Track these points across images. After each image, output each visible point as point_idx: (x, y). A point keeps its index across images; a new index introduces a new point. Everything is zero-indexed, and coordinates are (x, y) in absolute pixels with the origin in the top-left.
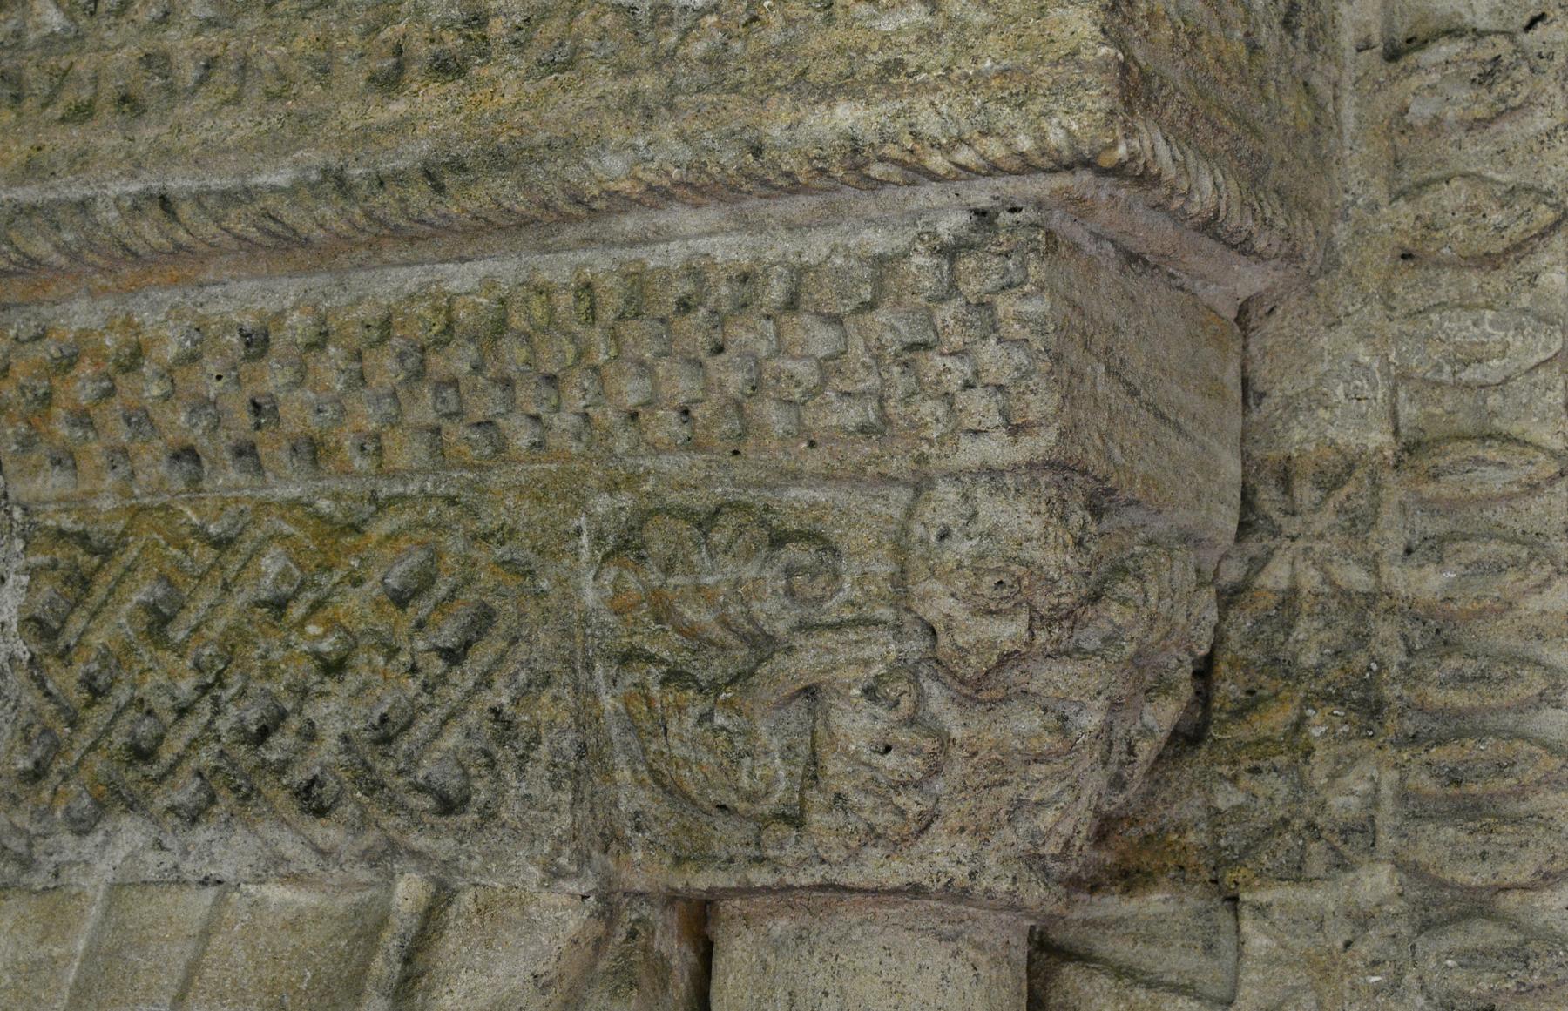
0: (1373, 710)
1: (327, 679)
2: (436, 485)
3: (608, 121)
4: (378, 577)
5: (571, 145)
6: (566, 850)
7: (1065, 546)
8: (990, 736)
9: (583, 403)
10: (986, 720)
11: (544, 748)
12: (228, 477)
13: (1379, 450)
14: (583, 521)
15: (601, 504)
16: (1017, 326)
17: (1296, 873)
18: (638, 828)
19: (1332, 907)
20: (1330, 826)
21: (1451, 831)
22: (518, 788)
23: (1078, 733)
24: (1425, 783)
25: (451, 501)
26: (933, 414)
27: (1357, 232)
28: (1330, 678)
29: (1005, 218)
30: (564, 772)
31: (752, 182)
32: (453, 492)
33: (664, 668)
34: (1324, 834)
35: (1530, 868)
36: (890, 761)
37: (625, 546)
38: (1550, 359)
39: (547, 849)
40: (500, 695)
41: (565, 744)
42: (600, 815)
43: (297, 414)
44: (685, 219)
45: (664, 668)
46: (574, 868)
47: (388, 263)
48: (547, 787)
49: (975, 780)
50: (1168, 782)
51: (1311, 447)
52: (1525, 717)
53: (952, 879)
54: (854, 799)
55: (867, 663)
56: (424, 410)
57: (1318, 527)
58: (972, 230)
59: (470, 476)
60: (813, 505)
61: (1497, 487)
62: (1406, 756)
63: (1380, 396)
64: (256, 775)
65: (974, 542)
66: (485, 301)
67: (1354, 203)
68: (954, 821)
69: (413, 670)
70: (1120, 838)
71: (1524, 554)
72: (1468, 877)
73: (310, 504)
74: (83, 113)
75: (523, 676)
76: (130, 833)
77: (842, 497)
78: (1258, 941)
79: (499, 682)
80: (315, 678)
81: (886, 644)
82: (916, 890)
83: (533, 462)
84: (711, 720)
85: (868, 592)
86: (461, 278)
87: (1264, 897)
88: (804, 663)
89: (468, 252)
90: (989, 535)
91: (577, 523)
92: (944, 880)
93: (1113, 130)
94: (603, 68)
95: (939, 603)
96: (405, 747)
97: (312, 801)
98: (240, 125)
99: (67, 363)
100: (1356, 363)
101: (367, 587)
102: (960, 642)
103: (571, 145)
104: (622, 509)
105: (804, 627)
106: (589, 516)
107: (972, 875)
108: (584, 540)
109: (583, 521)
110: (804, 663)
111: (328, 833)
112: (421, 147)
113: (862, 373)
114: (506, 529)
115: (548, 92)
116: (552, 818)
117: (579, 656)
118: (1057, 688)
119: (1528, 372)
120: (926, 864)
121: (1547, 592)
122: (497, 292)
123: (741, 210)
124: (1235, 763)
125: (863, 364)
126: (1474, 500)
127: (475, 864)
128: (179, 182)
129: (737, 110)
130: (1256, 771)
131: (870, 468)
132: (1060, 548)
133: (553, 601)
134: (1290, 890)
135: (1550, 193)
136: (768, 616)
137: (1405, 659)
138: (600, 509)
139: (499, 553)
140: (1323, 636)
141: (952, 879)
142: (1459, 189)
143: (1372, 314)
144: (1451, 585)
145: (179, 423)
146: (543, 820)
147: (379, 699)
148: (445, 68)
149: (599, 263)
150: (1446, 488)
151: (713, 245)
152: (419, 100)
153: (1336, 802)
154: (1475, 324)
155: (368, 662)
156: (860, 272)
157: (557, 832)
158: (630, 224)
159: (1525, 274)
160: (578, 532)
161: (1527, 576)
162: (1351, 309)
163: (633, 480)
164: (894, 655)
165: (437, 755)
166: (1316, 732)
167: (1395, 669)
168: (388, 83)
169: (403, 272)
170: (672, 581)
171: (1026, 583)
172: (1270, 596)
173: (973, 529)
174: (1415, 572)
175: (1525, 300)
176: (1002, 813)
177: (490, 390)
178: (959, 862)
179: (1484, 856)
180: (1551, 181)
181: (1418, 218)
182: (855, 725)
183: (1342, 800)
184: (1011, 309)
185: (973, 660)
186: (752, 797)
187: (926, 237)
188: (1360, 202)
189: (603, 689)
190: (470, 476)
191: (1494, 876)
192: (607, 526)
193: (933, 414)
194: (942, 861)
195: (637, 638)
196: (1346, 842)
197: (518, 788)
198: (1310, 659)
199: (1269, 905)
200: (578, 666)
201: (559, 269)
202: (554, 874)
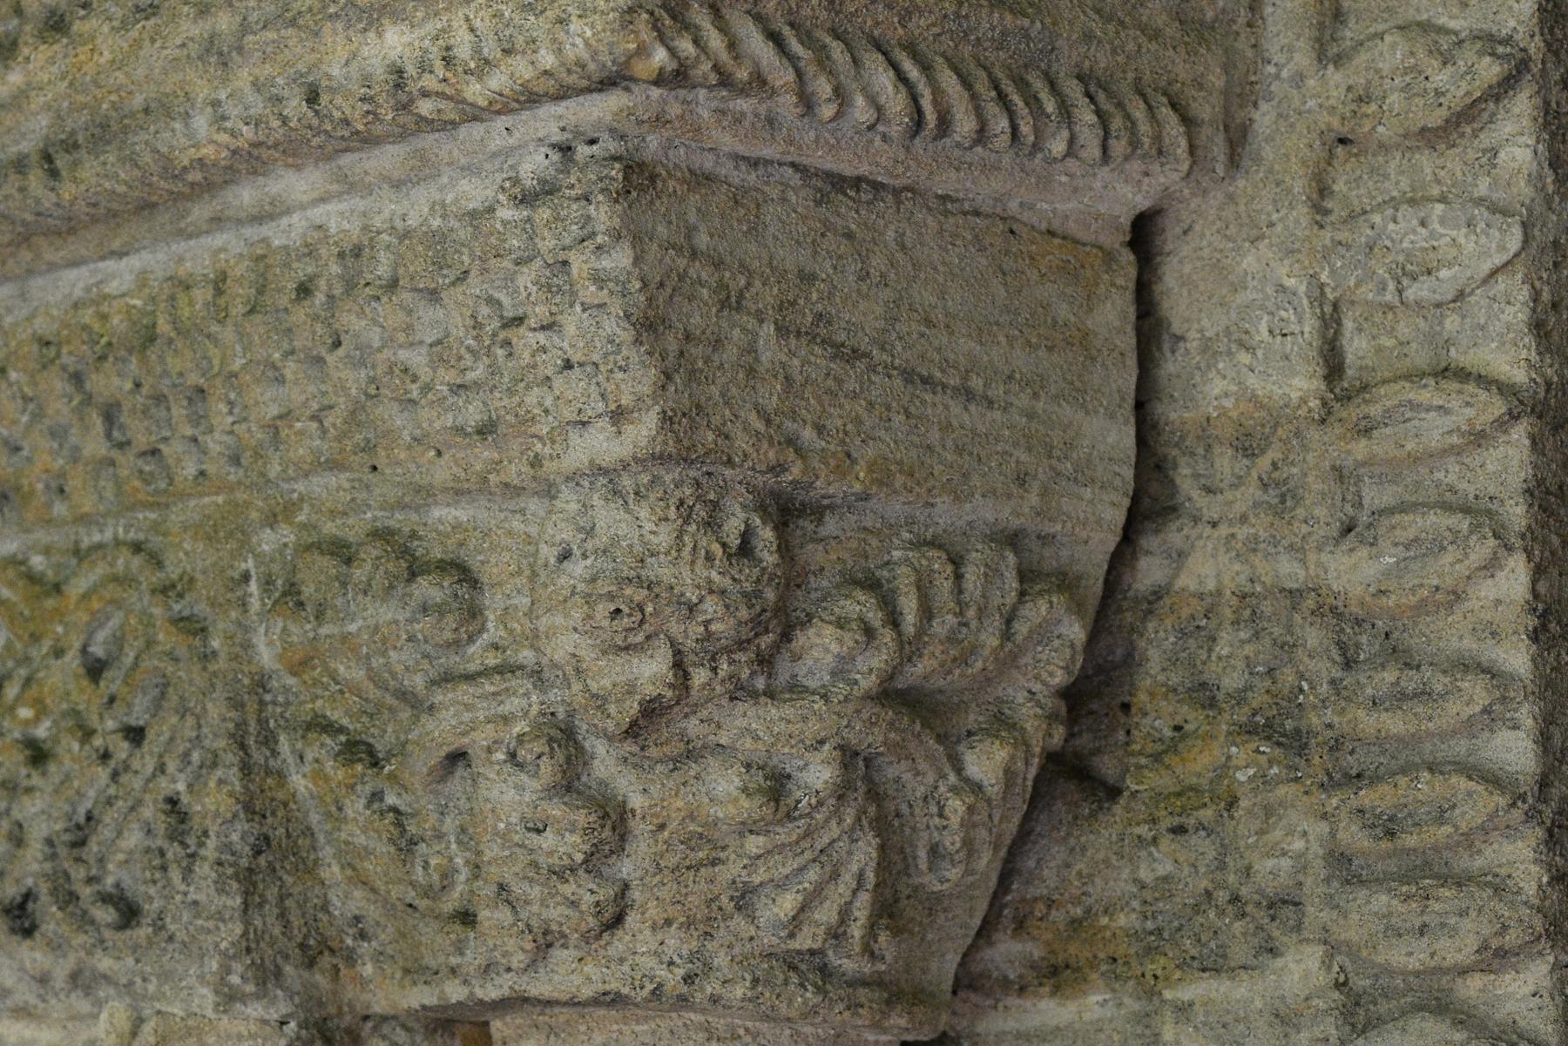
1: (34, 773)
2: (127, 528)
3: (191, 75)
4: (77, 645)
5: (162, 109)
6: (238, 967)
7: (709, 558)
8: (680, 804)
9: (230, 419)
10: (671, 784)
11: (211, 843)
13: (1304, 401)
14: (250, 564)
15: (268, 541)
16: (593, 288)
17: (1214, 966)
18: (363, 935)
19: (1258, 1004)
20: (1256, 897)
21: (1384, 898)
22: (185, 894)
23: (798, 794)
24: (1353, 836)
25: (137, 548)
26: (540, 404)
27: (1280, 115)
28: (1255, 704)
29: (583, 151)
30: (230, 871)
31: (324, 132)
32: (141, 536)
33: (343, 738)
34: (1249, 909)
35: (1472, 943)
36: (548, 840)
38: (1508, 263)
39: (215, 966)
40: (174, 781)
41: (235, 837)
42: (296, 922)
44: (296, 184)
45: (343, 738)
46: (250, 988)
47: (52, 267)
48: (212, 891)
49: (671, 860)
50: (1084, 849)
51: (1228, 403)
52: (1479, 742)
53: (660, 985)
54: (518, 888)
55: (506, 719)
57: (1240, 508)
58: (559, 171)
59: (153, 516)
60: (457, 527)
61: (1434, 440)
62: (1334, 802)
63: (1307, 329)
65: (589, 562)
66: (138, 303)
67: (1277, 76)
68: (653, 912)
69: (105, 756)
70: (1043, 925)
71: (1465, 526)
72: (1403, 959)
73: (22, 563)
75: (196, 756)
77: (482, 515)
79: (171, 767)
80: (24, 771)
81: (527, 695)
82: (612, 1000)
83: (202, 495)
84: (382, 800)
85: (512, 631)
87: (1185, 993)
88: (445, 725)
89: (116, 244)
90: (604, 552)
91: (243, 566)
92: (650, 987)
93: (636, 33)
94: (186, 9)
96: (95, 849)
100: (1281, 288)
101: (68, 658)
102: (594, 686)
103: (162, 109)
104: (285, 545)
105: (447, 679)
106: (256, 556)
107: (688, 979)
108: (253, 587)
109: (250, 564)
110: (445, 725)
113: (468, 360)
114: (186, 578)
115: (137, 44)
116: (218, 928)
117: (253, 727)
118: (757, 738)
119: (1485, 281)
120: (626, 968)
121: (1501, 575)
122: (147, 291)
123: (340, 168)
124: (1154, 821)
125: (468, 348)
126: (1416, 459)
127: (151, 988)
129: (297, 46)
130: (1179, 830)
131: (491, 477)
132: (700, 562)
133: (221, 664)
134: (1214, 983)
135: (1507, 41)
136: (407, 668)
137: (1337, 673)
138: (266, 547)
139: (177, 607)
140: (1248, 650)
141: (660, 985)
142: (1394, 46)
143: (1297, 221)
144: (1387, 574)
146: (209, 931)
147: (78, 793)
150: (1380, 445)
151: (328, 214)
152: (31, 66)
153: (1264, 866)
154: (1423, 224)
156: (462, 233)
157: (224, 945)
158: (245, 195)
159: (1484, 151)
160: (246, 577)
161: (1466, 555)
162: (1275, 216)
163: (290, 508)
164: (535, 710)
165: (121, 857)
166: (1241, 776)
167: (1324, 689)
169: (72, 274)
170: (323, 631)
171: (649, 609)
172: (1194, 601)
173: (589, 545)
174: (1345, 559)
175: (1483, 187)
176: (724, 900)
177: (154, 410)
178: (671, 963)
179: (1423, 930)
180: (1512, 23)
181: (1349, 89)
183: (1270, 863)
184: (585, 267)
185: (612, 709)
186: (427, 892)
187: (507, 184)
188: (1285, 74)
189: (292, 769)
190: (153, 516)
191: (1432, 955)
192: (275, 568)
193: (540, 404)
194: (649, 963)
195: (319, 703)
196: (1273, 919)
197: (185, 894)
198: (1232, 681)
199: (1191, 1004)
200: (251, 741)
201: (197, 256)
202: (229, 998)
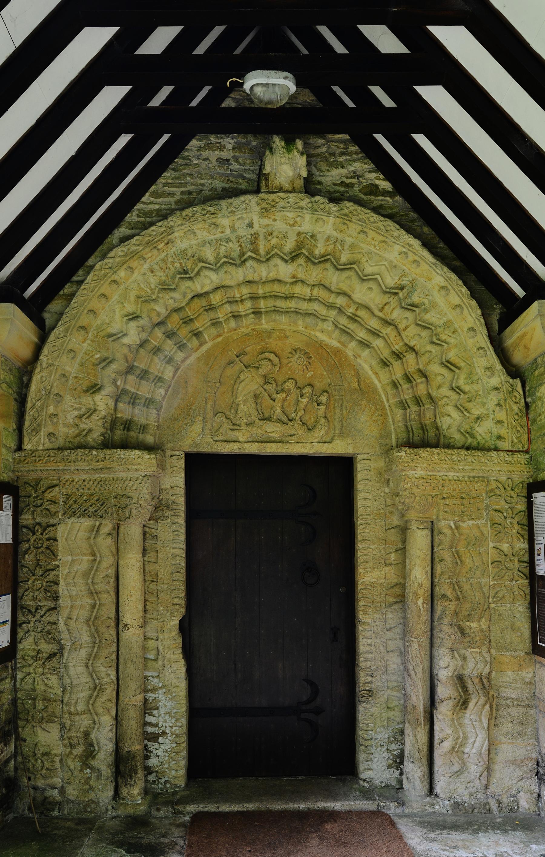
0: (169, 507)
12: (81, 491)
37: (116, 497)
43: (88, 486)
56: (99, 486)
64: (84, 514)
74: (70, 462)
76: (73, 519)
78: (160, 525)
86: (102, 476)
95: (141, 502)
97: (89, 516)
98: (85, 464)
99: (67, 481)
111: (91, 519)
112: (100, 467)
128: (79, 468)
129: (127, 466)
145: (77, 486)
148: (102, 461)
149: (114, 476)
155: (94, 506)
168: (98, 461)
182: (134, 511)
